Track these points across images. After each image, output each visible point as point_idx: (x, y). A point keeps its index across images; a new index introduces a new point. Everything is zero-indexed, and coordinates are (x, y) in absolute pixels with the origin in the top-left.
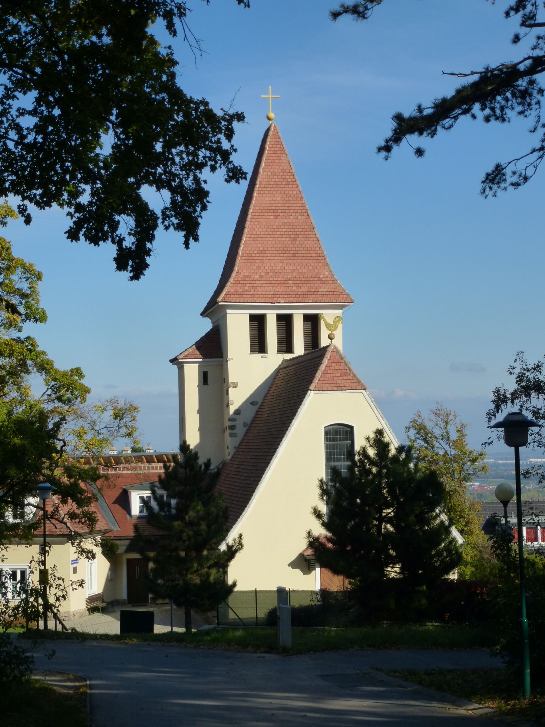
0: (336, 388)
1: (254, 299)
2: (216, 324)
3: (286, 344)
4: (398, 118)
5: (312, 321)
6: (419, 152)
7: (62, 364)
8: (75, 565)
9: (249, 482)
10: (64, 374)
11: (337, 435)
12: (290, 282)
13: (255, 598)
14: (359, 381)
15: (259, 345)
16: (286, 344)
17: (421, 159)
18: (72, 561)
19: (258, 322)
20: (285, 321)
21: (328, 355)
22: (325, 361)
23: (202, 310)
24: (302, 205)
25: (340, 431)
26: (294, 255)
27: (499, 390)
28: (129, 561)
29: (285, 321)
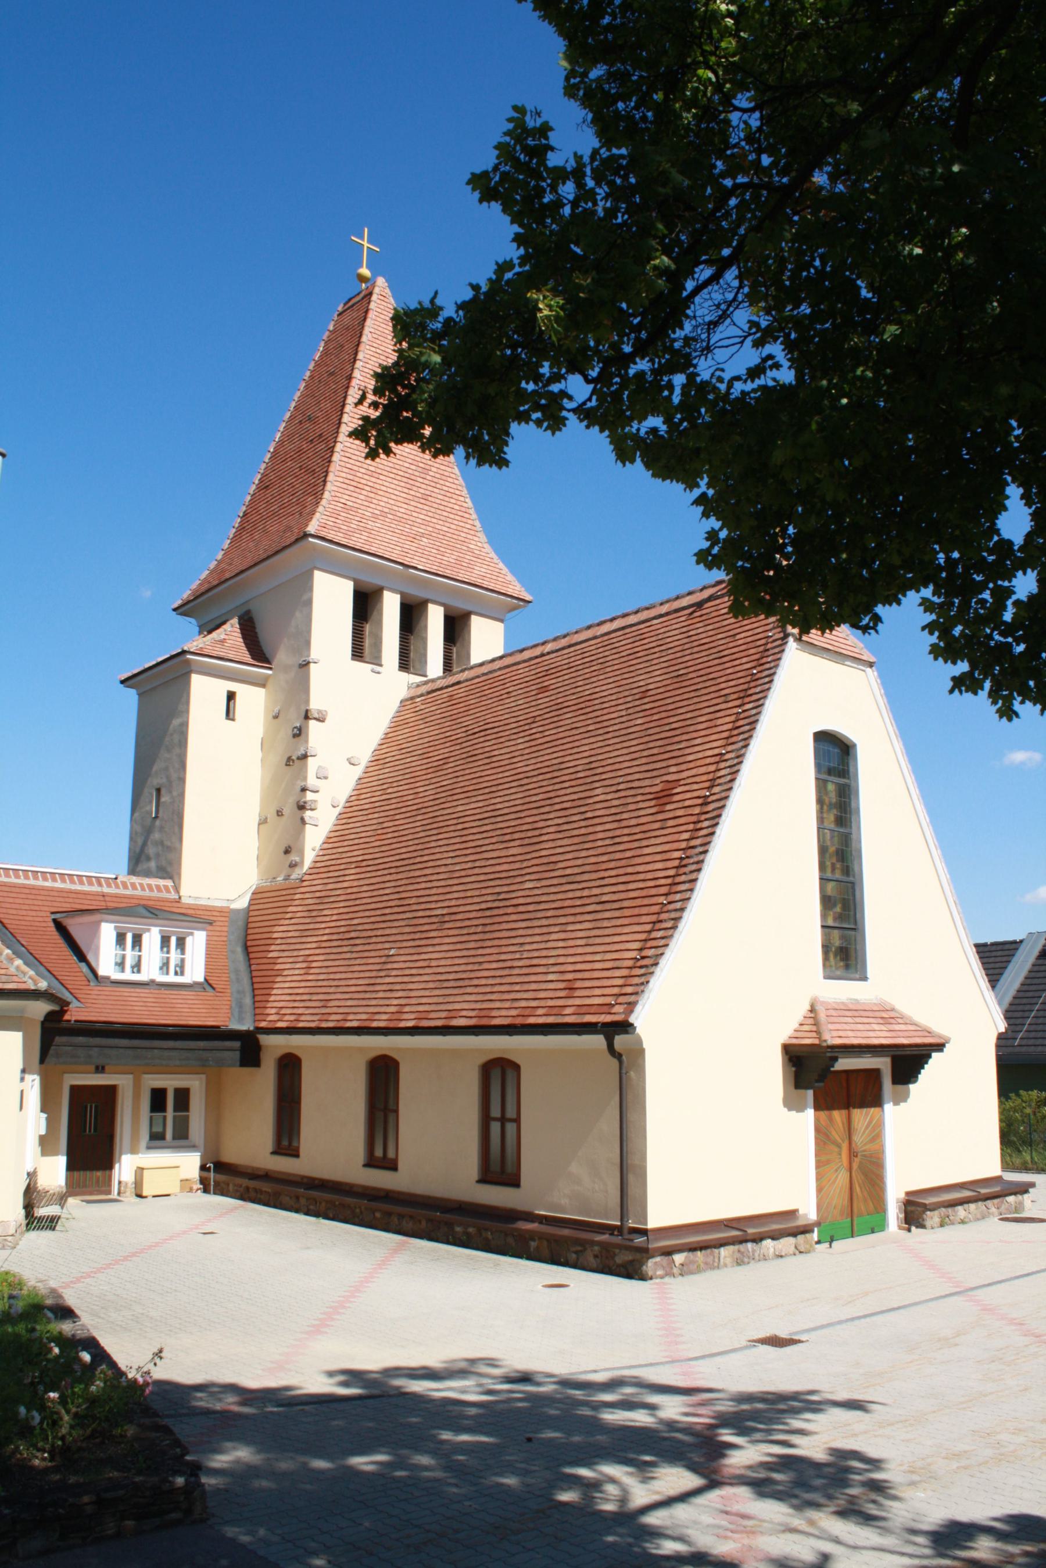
3: (409, 659)
19: (365, 605)
20: (411, 616)
26: (425, 497)
28: (74, 1089)
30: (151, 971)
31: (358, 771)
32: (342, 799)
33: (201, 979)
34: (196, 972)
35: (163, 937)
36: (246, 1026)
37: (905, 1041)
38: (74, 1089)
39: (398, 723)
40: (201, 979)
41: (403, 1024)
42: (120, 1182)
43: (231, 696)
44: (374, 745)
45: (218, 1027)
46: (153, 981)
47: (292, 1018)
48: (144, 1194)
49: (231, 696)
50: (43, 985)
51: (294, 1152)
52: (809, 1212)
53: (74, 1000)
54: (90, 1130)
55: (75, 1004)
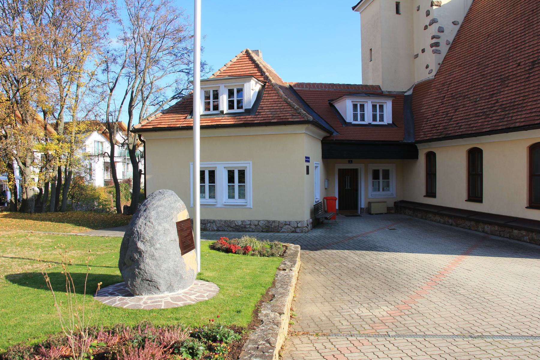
28: (340, 170)
30: (368, 120)
31: (457, 27)
32: (451, 40)
33: (391, 122)
34: (388, 119)
35: (373, 105)
36: (411, 140)
37: (364, 252)
38: (340, 170)
39: (344, 85)
40: (391, 122)
41: (484, 130)
42: (361, 208)
45: (398, 141)
46: (370, 124)
47: (431, 135)
48: (372, 212)
50: (311, 118)
51: (383, 121)
52: (121, 234)
53: (335, 132)
54: (348, 187)
55: (335, 134)
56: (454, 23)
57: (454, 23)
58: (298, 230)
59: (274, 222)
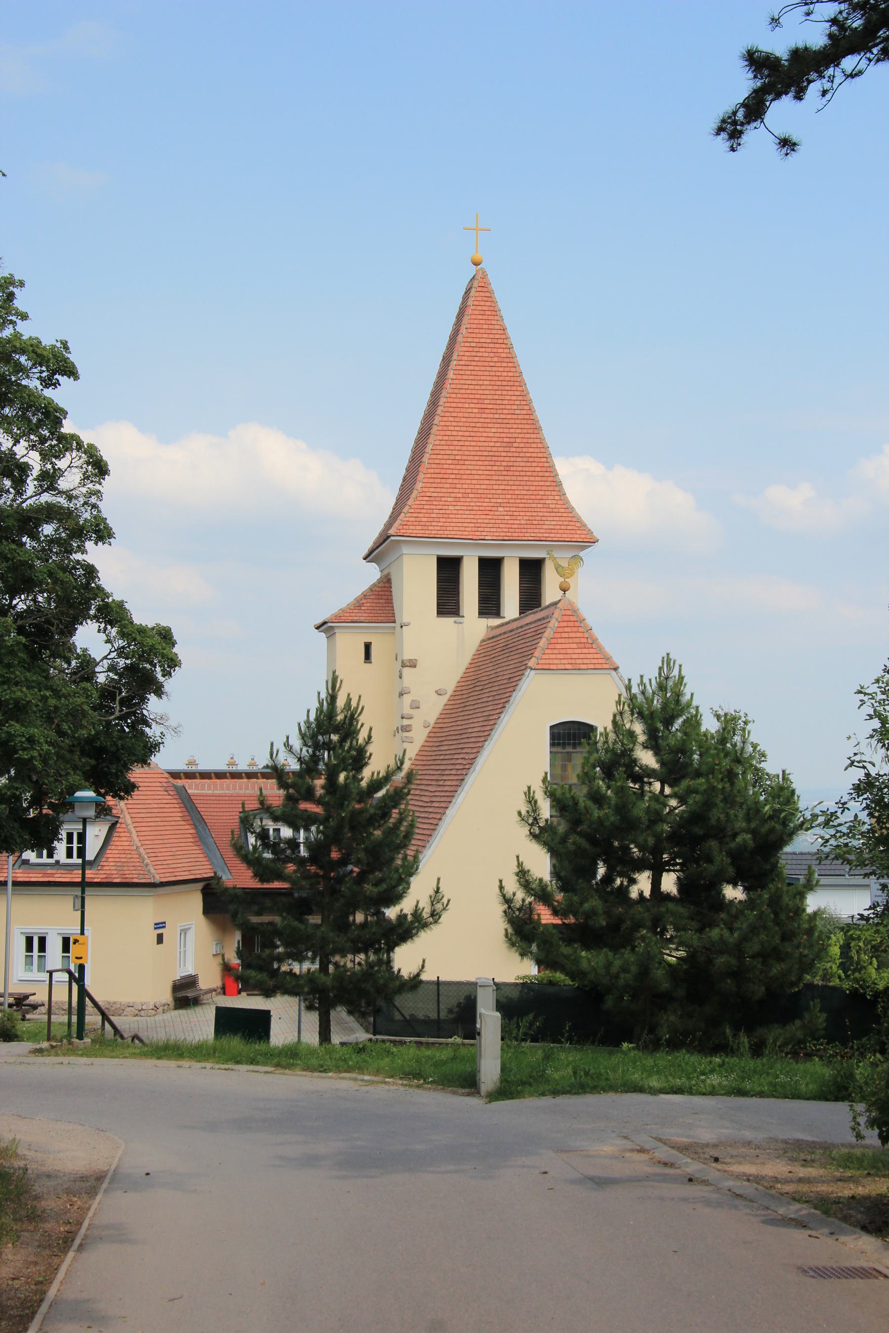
0: (569, 667)
1: (446, 532)
2: (385, 572)
3: (490, 603)
4: (757, 61)
5: (532, 570)
6: (787, 144)
7: (143, 616)
8: (160, 931)
9: (431, 810)
10: (142, 630)
11: (569, 739)
12: (501, 509)
13: (436, 993)
14: (608, 658)
15: (448, 603)
16: (490, 603)
17: (793, 156)
18: (156, 924)
19: (449, 569)
20: (490, 569)
21: (557, 614)
22: (553, 623)
23: (365, 552)
24: (522, 393)
25: (574, 734)
26: (508, 468)
27: (27, 1170)
29: (490, 569)
31: (444, 699)
32: (432, 720)
43: (368, 647)
44: (458, 678)
49: (368, 647)
56: (439, 693)
57: (439, 693)
58: (142, 1013)
59: (115, 1003)
